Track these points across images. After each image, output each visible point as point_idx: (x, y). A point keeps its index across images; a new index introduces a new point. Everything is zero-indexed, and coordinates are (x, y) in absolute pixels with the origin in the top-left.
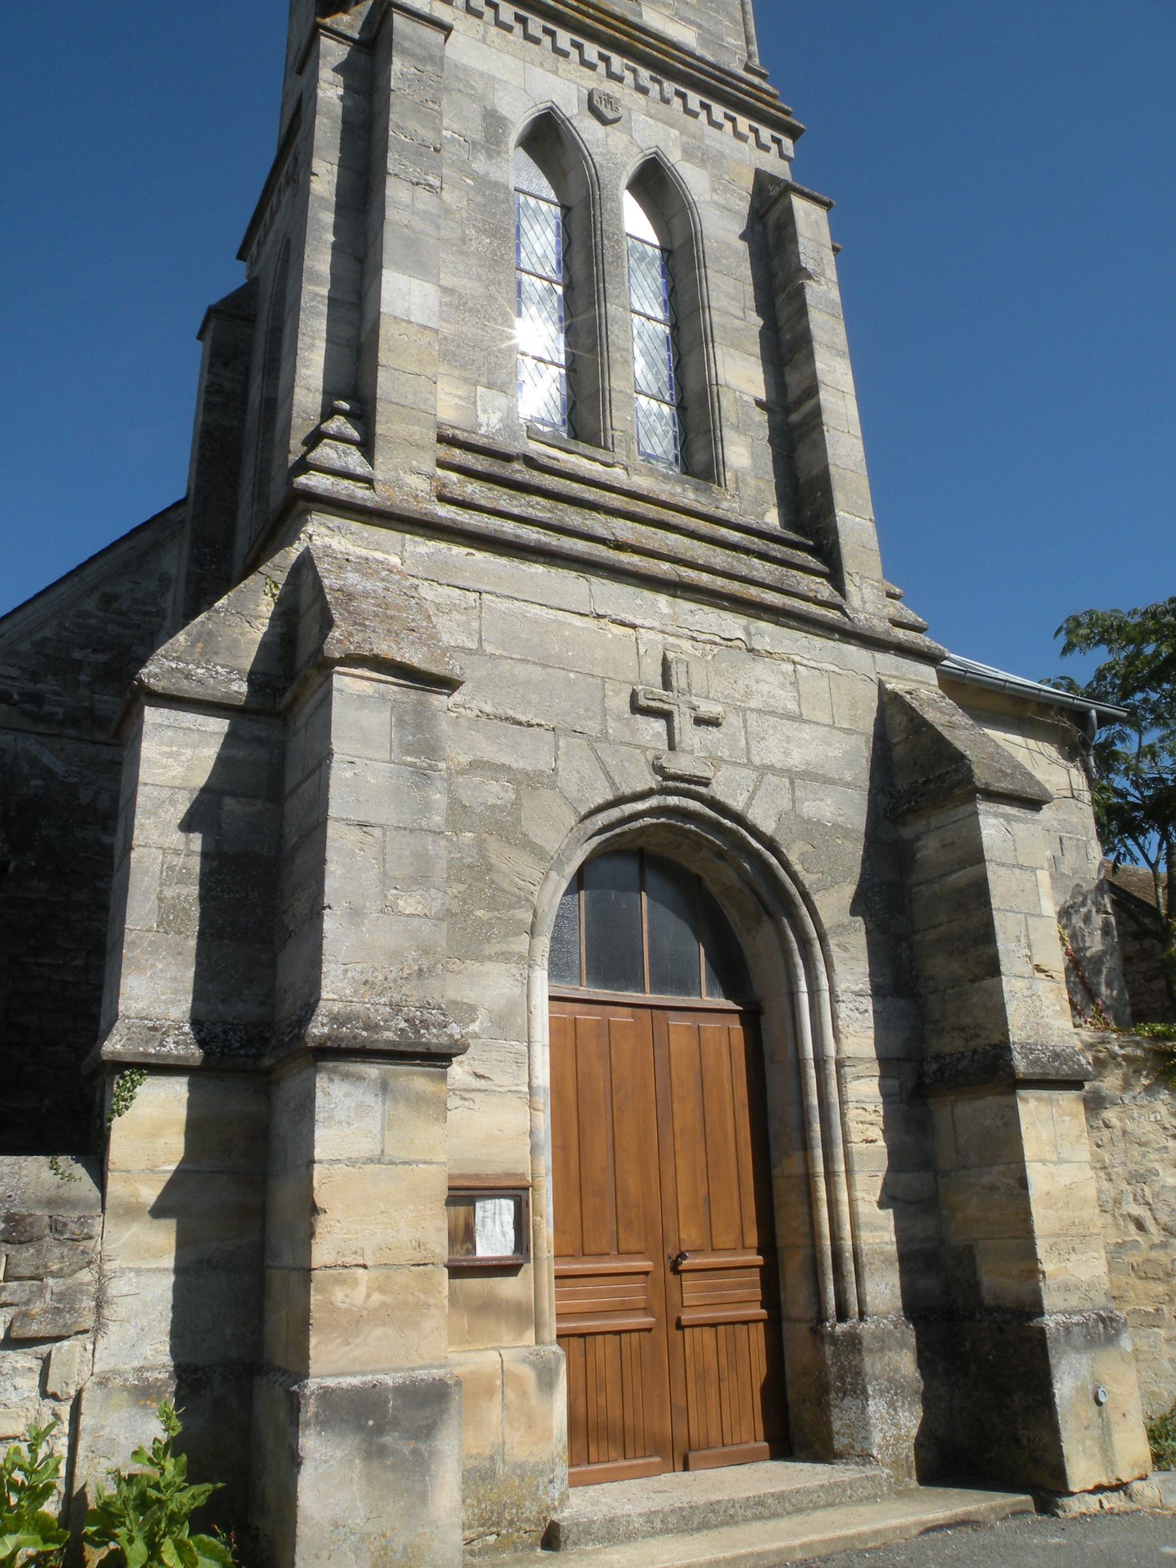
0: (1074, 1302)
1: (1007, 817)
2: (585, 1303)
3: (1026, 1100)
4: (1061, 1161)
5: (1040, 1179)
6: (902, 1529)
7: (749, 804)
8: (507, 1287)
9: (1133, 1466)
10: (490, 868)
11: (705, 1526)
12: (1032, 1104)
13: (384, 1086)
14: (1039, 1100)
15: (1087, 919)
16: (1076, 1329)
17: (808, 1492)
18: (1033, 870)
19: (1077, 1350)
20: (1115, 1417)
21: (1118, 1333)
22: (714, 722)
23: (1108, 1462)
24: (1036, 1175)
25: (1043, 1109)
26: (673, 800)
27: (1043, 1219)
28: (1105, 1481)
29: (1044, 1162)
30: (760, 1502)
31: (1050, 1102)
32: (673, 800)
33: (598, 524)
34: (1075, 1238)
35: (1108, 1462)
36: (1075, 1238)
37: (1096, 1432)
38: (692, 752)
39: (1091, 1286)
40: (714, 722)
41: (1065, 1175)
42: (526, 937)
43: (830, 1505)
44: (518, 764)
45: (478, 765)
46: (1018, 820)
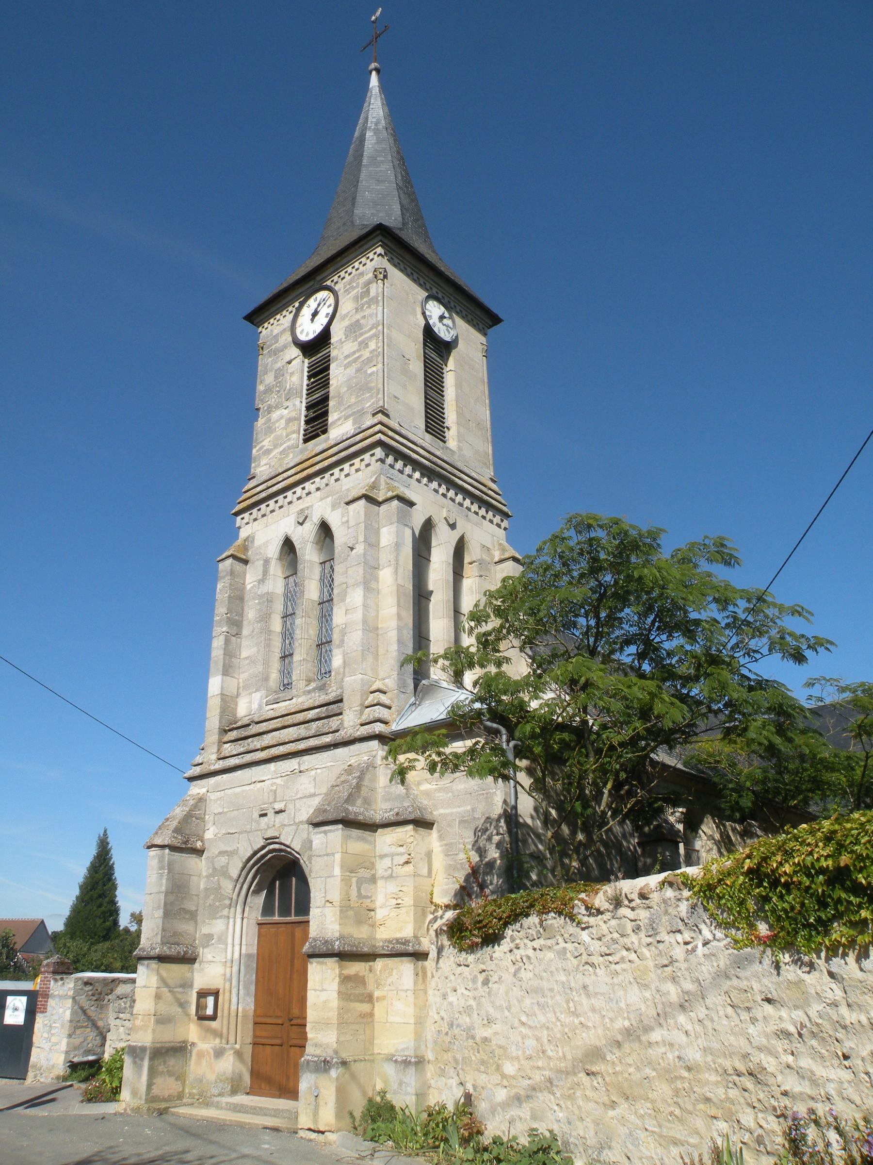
0: (318, 1052)
1: (325, 832)
2: (264, 1034)
3: (312, 963)
4: (323, 990)
5: (312, 997)
6: (257, 1124)
7: (292, 841)
8: (214, 1024)
9: (326, 1125)
10: (220, 887)
11: (240, 1111)
12: (314, 964)
13: (148, 966)
14: (318, 963)
15: (489, 839)
16: (311, 1063)
17: (269, 1109)
18: (333, 854)
19: (311, 1072)
20: (322, 1103)
21: (330, 1068)
22: (281, 811)
23: (316, 1121)
24: (311, 996)
25: (319, 967)
26: (272, 847)
27: (311, 1015)
28: (312, 1127)
29: (315, 990)
30: (255, 1108)
31: (322, 963)
32: (272, 847)
33: (267, 740)
34: (324, 1024)
35: (316, 1121)
36: (324, 1024)
37: (312, 1107)
38: (653, 695)
39: (327, 1045)
40: (281, 811)
41: (324, 996)
42: (227, 910)
43: (275, 1116)
44: (229, 849)
45: (222, 853)
46: (330, 831)
